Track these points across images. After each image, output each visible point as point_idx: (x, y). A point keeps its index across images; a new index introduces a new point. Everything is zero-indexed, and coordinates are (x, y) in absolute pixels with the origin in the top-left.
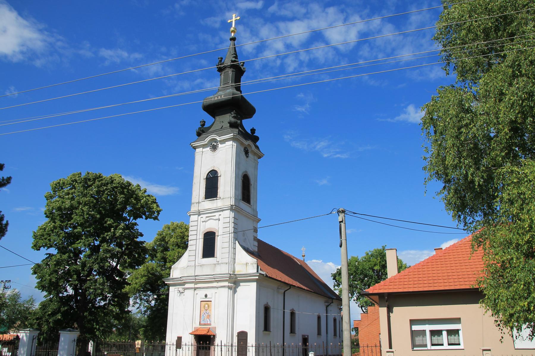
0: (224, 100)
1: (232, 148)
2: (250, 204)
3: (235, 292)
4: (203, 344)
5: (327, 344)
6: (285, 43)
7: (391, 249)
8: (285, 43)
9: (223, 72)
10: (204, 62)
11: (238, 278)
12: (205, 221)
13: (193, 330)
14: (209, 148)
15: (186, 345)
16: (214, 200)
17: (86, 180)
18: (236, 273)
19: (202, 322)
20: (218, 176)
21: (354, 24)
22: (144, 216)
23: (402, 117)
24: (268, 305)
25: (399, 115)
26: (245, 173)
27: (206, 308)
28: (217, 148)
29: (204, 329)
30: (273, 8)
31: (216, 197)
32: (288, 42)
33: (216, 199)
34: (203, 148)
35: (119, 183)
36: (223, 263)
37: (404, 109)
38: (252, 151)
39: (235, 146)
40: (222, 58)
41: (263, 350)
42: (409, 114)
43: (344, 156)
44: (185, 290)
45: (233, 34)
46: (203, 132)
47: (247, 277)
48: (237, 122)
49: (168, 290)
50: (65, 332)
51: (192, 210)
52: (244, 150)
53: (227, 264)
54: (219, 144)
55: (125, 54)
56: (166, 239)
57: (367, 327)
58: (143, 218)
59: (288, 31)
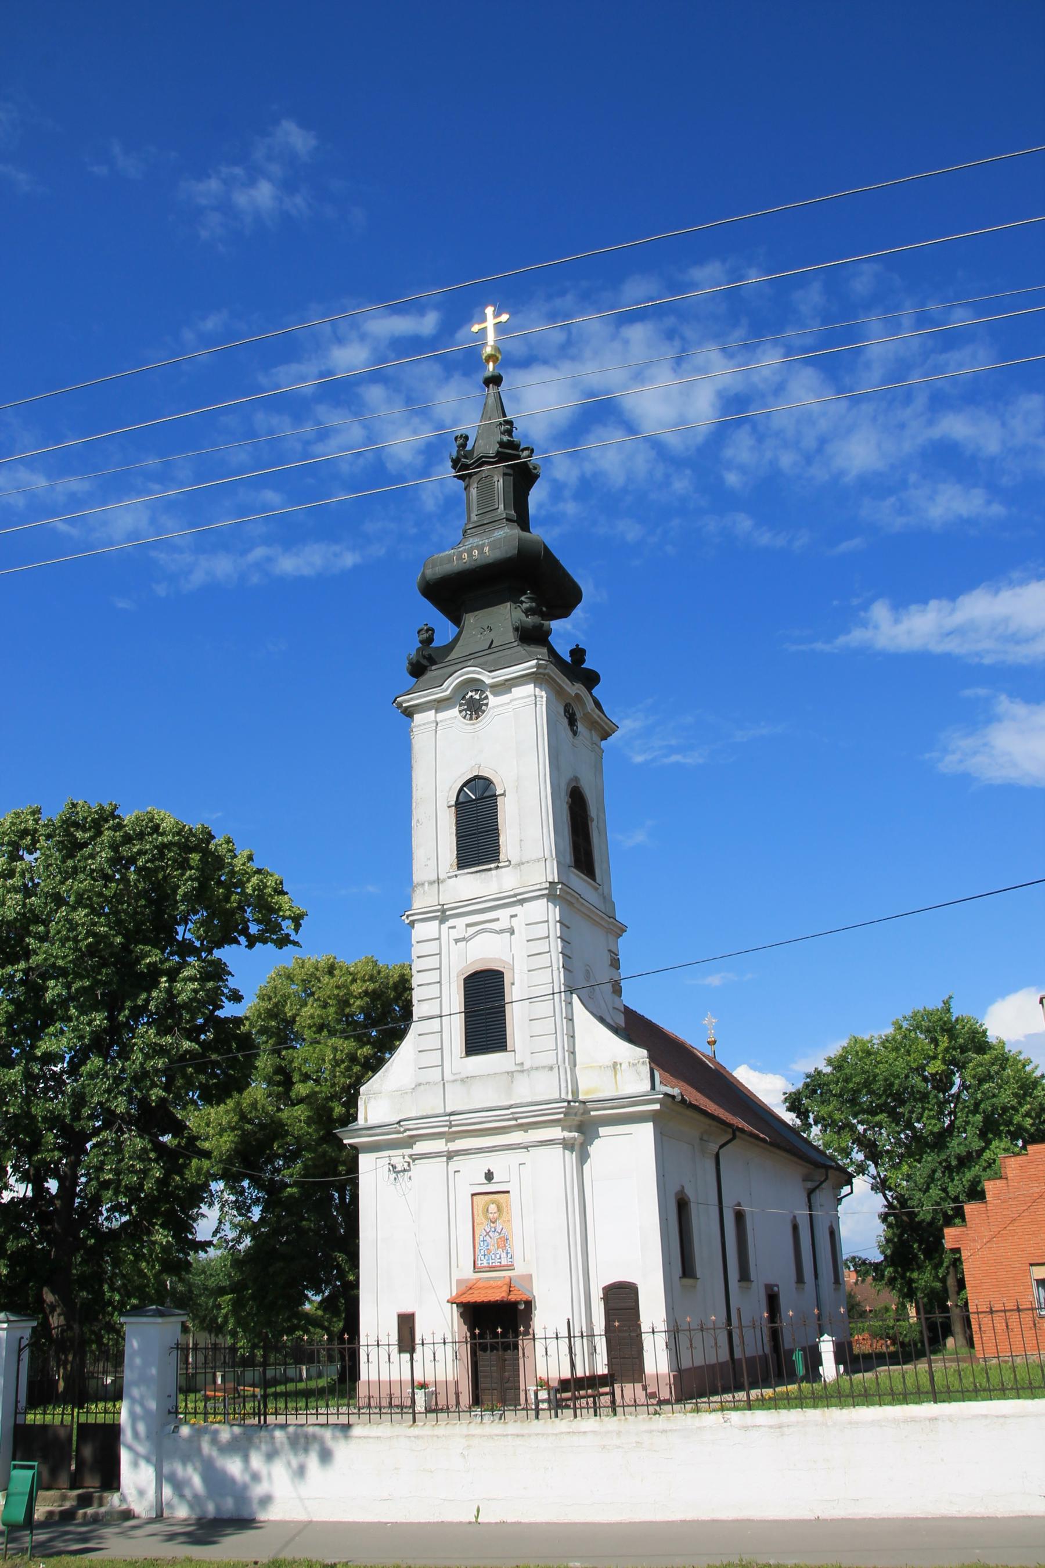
0: (491, 561)
1: (536, 704)
2: (594, 880)
3: (583, 1157)
4: (504, 1335)
10: (270, 496)
11: (592, 1113)
12: (464, 939)
13: (454, 1294)
15: (557, 1338)
16: (490, 870)
17: (70, 824)
18: (581, 1097)
19: (483, 1262)
20: (495, 795)
22: (242, 939)
23: (857, 636)
24: (686, 1194)
25: (848, 632)
26: (574, 784)
27: (491, 1216)
29: (493, 1283)
31: (498, 860)
33: (497, 867)
34: (436, 712)
35: (178, 833)
36: (537, 1068)
37: (862, 614)
38: (587, 716)
39: (544, 699)
40: (466, 438)
42: (876, 627)
43: (691, 759)
44: (417, 1162)
45: (491, 366)
46: (432, 661)
50: (144, 1319)
52: (566, 711)
53: (551, 1068)
54: (491, 697)
55: (40, 482)
56: (287, 1009)
57: (988, 1245)
58: (238, 943)
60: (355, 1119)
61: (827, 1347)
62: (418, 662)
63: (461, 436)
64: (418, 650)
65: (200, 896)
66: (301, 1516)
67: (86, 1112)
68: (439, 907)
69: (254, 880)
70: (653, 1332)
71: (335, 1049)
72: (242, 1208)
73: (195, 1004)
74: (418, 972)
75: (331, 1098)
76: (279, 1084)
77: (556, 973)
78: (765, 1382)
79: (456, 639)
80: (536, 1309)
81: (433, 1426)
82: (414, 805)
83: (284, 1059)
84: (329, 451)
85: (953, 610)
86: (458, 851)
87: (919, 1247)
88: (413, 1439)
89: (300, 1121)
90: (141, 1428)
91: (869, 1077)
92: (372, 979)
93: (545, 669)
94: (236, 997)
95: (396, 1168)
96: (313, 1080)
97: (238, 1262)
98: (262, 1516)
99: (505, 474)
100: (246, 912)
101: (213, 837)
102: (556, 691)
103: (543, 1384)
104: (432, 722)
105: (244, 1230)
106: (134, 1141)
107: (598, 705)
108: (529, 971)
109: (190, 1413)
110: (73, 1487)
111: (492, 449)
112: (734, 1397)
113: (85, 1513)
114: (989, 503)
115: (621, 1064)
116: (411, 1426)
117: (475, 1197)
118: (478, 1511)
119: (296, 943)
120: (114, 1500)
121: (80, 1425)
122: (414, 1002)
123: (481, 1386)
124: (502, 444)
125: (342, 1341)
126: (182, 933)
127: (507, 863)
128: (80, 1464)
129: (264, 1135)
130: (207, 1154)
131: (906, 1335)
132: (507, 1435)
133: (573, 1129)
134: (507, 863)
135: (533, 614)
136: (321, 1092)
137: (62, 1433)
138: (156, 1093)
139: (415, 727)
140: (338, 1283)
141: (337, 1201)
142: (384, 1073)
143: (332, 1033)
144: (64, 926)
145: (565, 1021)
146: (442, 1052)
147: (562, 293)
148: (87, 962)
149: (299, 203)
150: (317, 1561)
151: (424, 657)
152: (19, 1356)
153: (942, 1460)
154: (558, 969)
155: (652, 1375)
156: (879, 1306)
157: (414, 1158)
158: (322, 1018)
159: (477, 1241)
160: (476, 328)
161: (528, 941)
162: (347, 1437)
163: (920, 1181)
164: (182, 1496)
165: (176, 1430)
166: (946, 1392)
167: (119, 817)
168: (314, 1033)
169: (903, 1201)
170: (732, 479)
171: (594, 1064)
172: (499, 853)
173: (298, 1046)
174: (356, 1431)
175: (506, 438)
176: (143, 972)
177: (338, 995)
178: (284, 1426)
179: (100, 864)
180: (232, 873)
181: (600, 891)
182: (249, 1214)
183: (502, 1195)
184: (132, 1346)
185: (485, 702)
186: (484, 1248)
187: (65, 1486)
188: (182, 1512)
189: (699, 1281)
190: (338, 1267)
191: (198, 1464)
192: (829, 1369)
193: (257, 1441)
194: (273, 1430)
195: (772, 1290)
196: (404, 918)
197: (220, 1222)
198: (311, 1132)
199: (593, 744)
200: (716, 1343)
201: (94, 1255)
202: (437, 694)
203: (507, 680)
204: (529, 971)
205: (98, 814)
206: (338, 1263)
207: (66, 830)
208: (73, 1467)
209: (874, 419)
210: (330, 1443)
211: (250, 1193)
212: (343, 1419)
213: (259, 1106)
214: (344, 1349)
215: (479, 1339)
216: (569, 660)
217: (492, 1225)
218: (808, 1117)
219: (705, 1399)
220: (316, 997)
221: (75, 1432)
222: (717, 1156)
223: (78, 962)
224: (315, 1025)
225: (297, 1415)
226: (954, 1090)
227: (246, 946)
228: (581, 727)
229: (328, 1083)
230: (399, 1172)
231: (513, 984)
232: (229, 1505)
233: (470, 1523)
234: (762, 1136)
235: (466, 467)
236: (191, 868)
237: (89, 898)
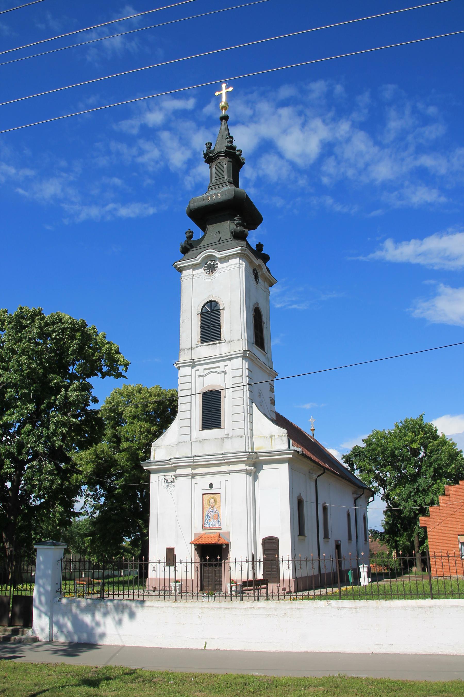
0: (221, 201)
1: (240, 267)
2: (264, 351)
3: (255, 479)
4: (210, 560)
9: (215, 163)
11: (260, 458)
13: (193, 540)
14: (203, 269)
16: (216, 344)
17: (20, 317)
18: (255, 451)
20: (219, 309)
21: (314, 131)
22: (99, 374)
23: (378, 254)
25: (374, 252)
26: (256, 306)
27: (211, 504)
33: (220, 343)
34: (193, 270)
35: (71, 323)
36: (235, 437)
37: (381, 244)
38: (263, 275)
39: (244, 265)
40: (211, 144)
41: (301, 566)
42: (387, 251)
46: (192, 247)
48: (244, 231)
49: (149, 477)
51: (181, 359)
52: (254, 272)
53: (242, 437)
54: (219, 264)
55: (12, 171)
57: (439, 526)
58: (98, 376)
60: (149, 458)
61: (364, 570)
62: (185, 247)
63: (209, 143)
64: (185, 241)
65: (80, 352)
66: (120, 643)
67: (24, 450)
68: (192, 360)
69: (107, 346)
71: (141, 427)
72: (96, 498)
73: (76, 402)
74: (181, 390)
75: (138, 449)
76: (114, 442)
77: (245, 392)
78: (334, 584)
79: (203, 237)
80: (231, 548)
81: (185, 602)
82: (181, 313)
83: (117, 431)
84: (144, 159)
85: (421, 244)
86: (201, 335)
87: (401, 526)
88: (175, 608)
89: (124, 459)
90: (43, 599)
91: (384, 448)
92: (158, 395)
94: (96, 401)
95: (167, 481)
96: (130, 441)
97: (93, 523)
98: (100, 643)
99: (228, 161)
100: (101, 361)
101: (87, 325)
102: (250, 262)
103: (232, 582)
104: (191, 275)
105: (96, 508)
106: (48, 466)
107: (268, 270)
108: (233, 391)
109: (67, 592)
110: (10, 625)
111: (223, 149)
113: (15, 638)
114: (440, 196)
115: (274, 436)
116: (174, 602)
117: (204, 495)
119: (125, 377)
120: (29, 632)
121: (14, 596)
122: (179, 404)
123: (204, 582)
124: (228, 147)
125: (142, 560)
126: (71, 369)
127: (224, 341)
128: (13, 614)
129: (107, 465)
130: (80, 472)
131: (393, 565)
132: (221, 608)
133: (251, 465)
134: (224, 341)
135: (240, 226)
136: (134, 446)
137: (5, 600)
138: (58, 443)
139: (183, 277)
140: (138, 534)
141: (139, 496)
142: (163, 437)
143: (139, 420)
144: (15, 364)
145: (249, 415)
146: (191, 428)
147: (252, 92)
148: (26, 381)
149: (133, 46)
150: (127, 667)
151: (188, 244)
153: (435, 627)
154: (247, 391)
155: (287, 580)
156: (379, 552)
157: (176, 476)
158: (135, 413)
159: (204, 516)
160: (217, 94)
161: (233, 377)
162: (142, 606)
163: (405, 496)
164: (62, 632)
165: (60, 600)
167: (43, 314)
168: (131, 419)
169: (396, 505)
170: (325, 180)
171: (262, 436)
172: (220, 336)
173: (124, 425)
174: (147, 604)
175: (229, 145)
176: (53, 386)
177: (143, 402)
178: (112, 600)
179: (33, 335)
180: (96, 343)
181: (266, 356)
182: (99, 501)
183: (217, 495)
185: (216, 266)
186: (207, 519)
187: (6, 625)
188: (62, 639)
190: (139, 526)
191: (70, 617)
192: (364, 580)
193: (99, 606)
194: (107, 602)
195: (338, 543)
196: (175, 365)
197: (85, 504)
198: (129, 465)
199: (265, 288)
200: (313, 567)
201: (26, 517)
202: (193, 261)
203: (227, 256)
205: (33, 312)
206: (139, 524)
207: (18, 320)
208: (10, 615)
209: (390, 156)
210: (134, 609)
211: (100, 491)
212: (141, 598)
213: (105, 452)
214: (142, 564)
215: (209, 561)
216: (255, 249)
217: (212, 508)
218: (354, 466)
220: (132, 403)
221: (12, 600)
222: (316, 481)
223: (22, 381)
224: (132, 415)
226: (421, 456)
227: (101, 377)
228: (260, 280)
229: (137, 442)
230: (169, 483)
231: (225, 397)
232: (84, 637)
233: (202, 649)
234: (336, 472)
235: (210, 157)
236: (76, 339)
237: (28, 351)
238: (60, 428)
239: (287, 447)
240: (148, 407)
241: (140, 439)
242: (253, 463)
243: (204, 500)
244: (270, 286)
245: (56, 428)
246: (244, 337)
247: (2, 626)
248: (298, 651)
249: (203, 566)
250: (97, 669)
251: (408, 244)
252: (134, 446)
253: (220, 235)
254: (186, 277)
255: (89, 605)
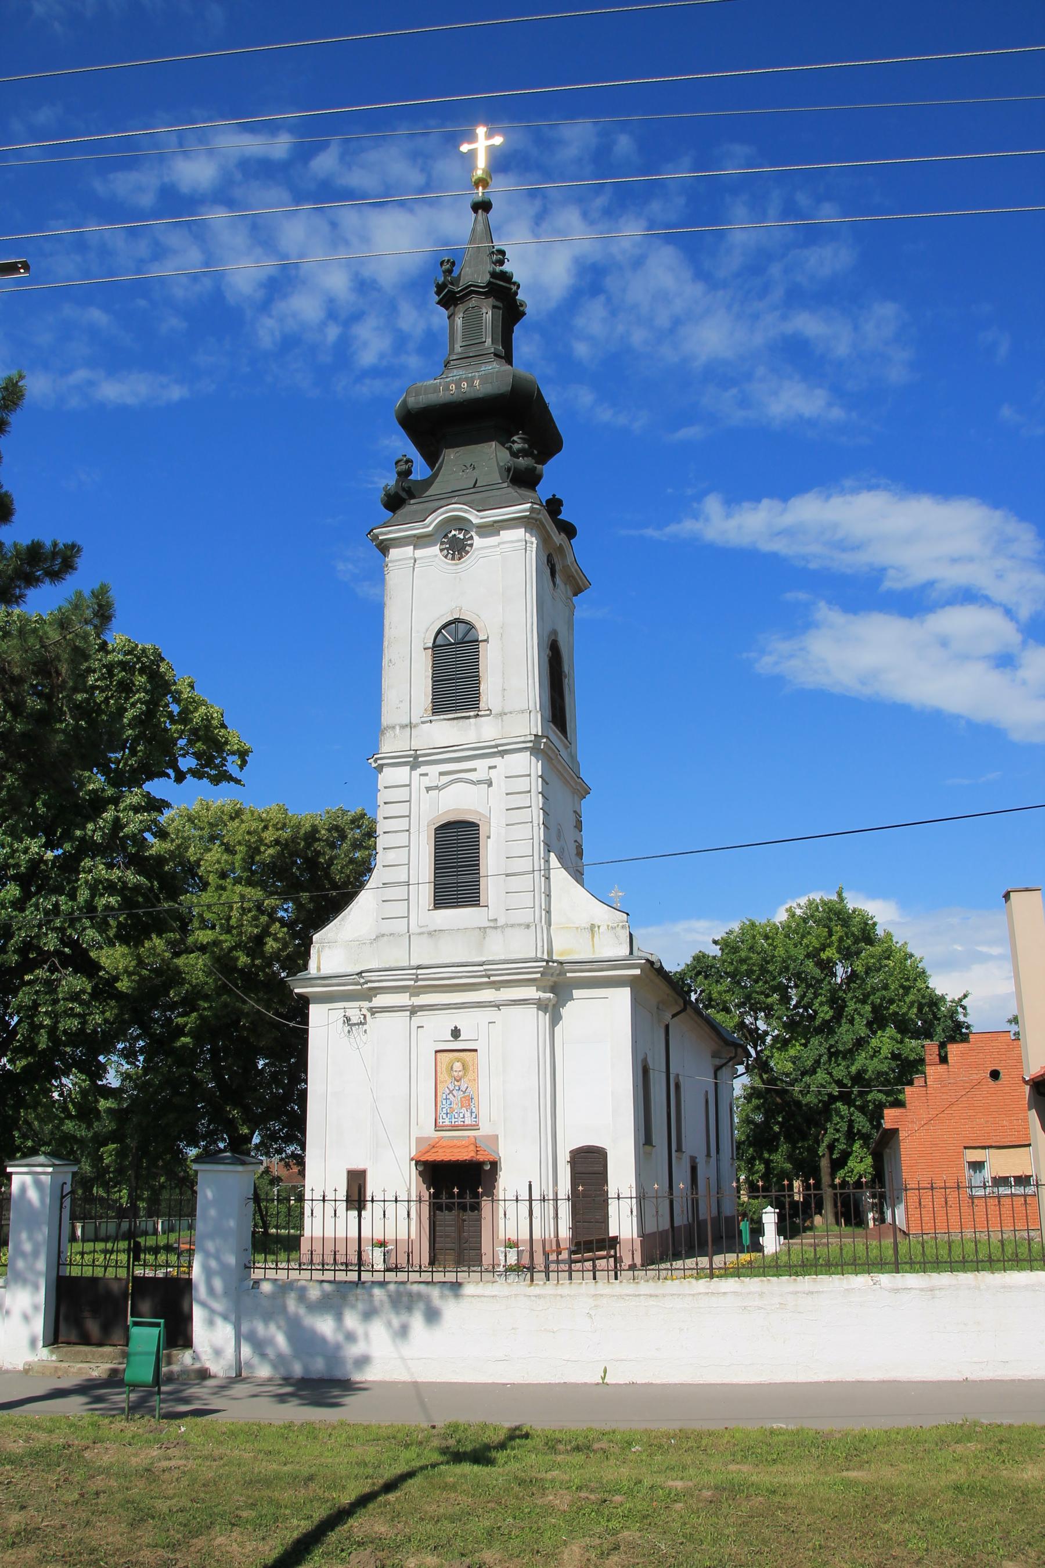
0: (481, 396)
4: (461, 1195)
5: (719, 1187)
6: (357, 274)
7: (1027, 890)
8: (357, 274)
9: (461, 308)
11: (568, 975)
14: (437, 547)
16: (469, 717)
20: (477, 641)
23: (688, 526)
27: (455, 1074)
28: (468, 548)
30: (325, 163)
32: (366, 273)
36: (512, 926)
37: (695, 505)
38: (566, 567)
39: (535, 546)
40: (453, 264)
42: (707, 520)
44: (377, 1015)
47: (461, 977)
50: (222, 1167)
53: (528, 926)
54: (476, 537)
57: (926, 1127)
58: (168, 776)
59: (365, 239)
60: (305, 967)
62: (396, 494)
63: (448, 261)
68: (413, 752)
70: (396, 1201)
77: (536, 829)
80: (501, 1171)
82: (386, 644)
90: (218, 1284)
93: (539, 514)
98: (357, 1377)
99: (494, 307)
102: (545, 541)
104: (410, 558)
108: (507, 825)
111: (484, 279)
112: (671, 1265)
115: (599, 927)
117: (438, 1054)
118: (605, 1371)
119: (238, 782)
120: (186, 1358)
124: (494, 275)
127: (488, 712)
132: (639, 1295)
133: (548, 990)
136: (226, 941)
137: (115, 1287)
139: (391, 561)
151: (404, 489)
152: (62, 1204)
154: (539, 824)
157: (373, 1011)
159: (439, 1099)
164: (263, 1355)
165: (255, 1286)
166: (988, 1261)
170: (581, 350)
174: (469, 1289)
184: (206, 1196)
185: (469, 542)
186: (446, 1106)
187: (121, 1343)
188: (264, 1371)
189: (654, 1149)
191: (282, 1323)
193: (352, 1298)
194: (371, 1287)
196: (371, 761)
199: (567, 598)
202: (417, 528)
204: (507, 825)
210: (436, 1301)
212: (451, 1277)
217: (456, 1083)
219: (668, 1265)
225: (445, 1272)
230: (355, 1024)
231: (489, 837)
232: (319, 1366)
233: (598, 1384)
238: (102, 895)
239: (628, 954)
240: (259, 852)
241: (242, 925)
242: (552, 984)
243: (439, 1064)
244: (575, 594)
245: (93, 896)
246: (533, 706)
247: (111, 1345)
248: (810, 1380)
249: (436, 1207)
250: (434, 1431)
251: (755, 509)
252: (226, 941)
253: (476, 473)
254: (397, 564)
255: (328, 1295)
